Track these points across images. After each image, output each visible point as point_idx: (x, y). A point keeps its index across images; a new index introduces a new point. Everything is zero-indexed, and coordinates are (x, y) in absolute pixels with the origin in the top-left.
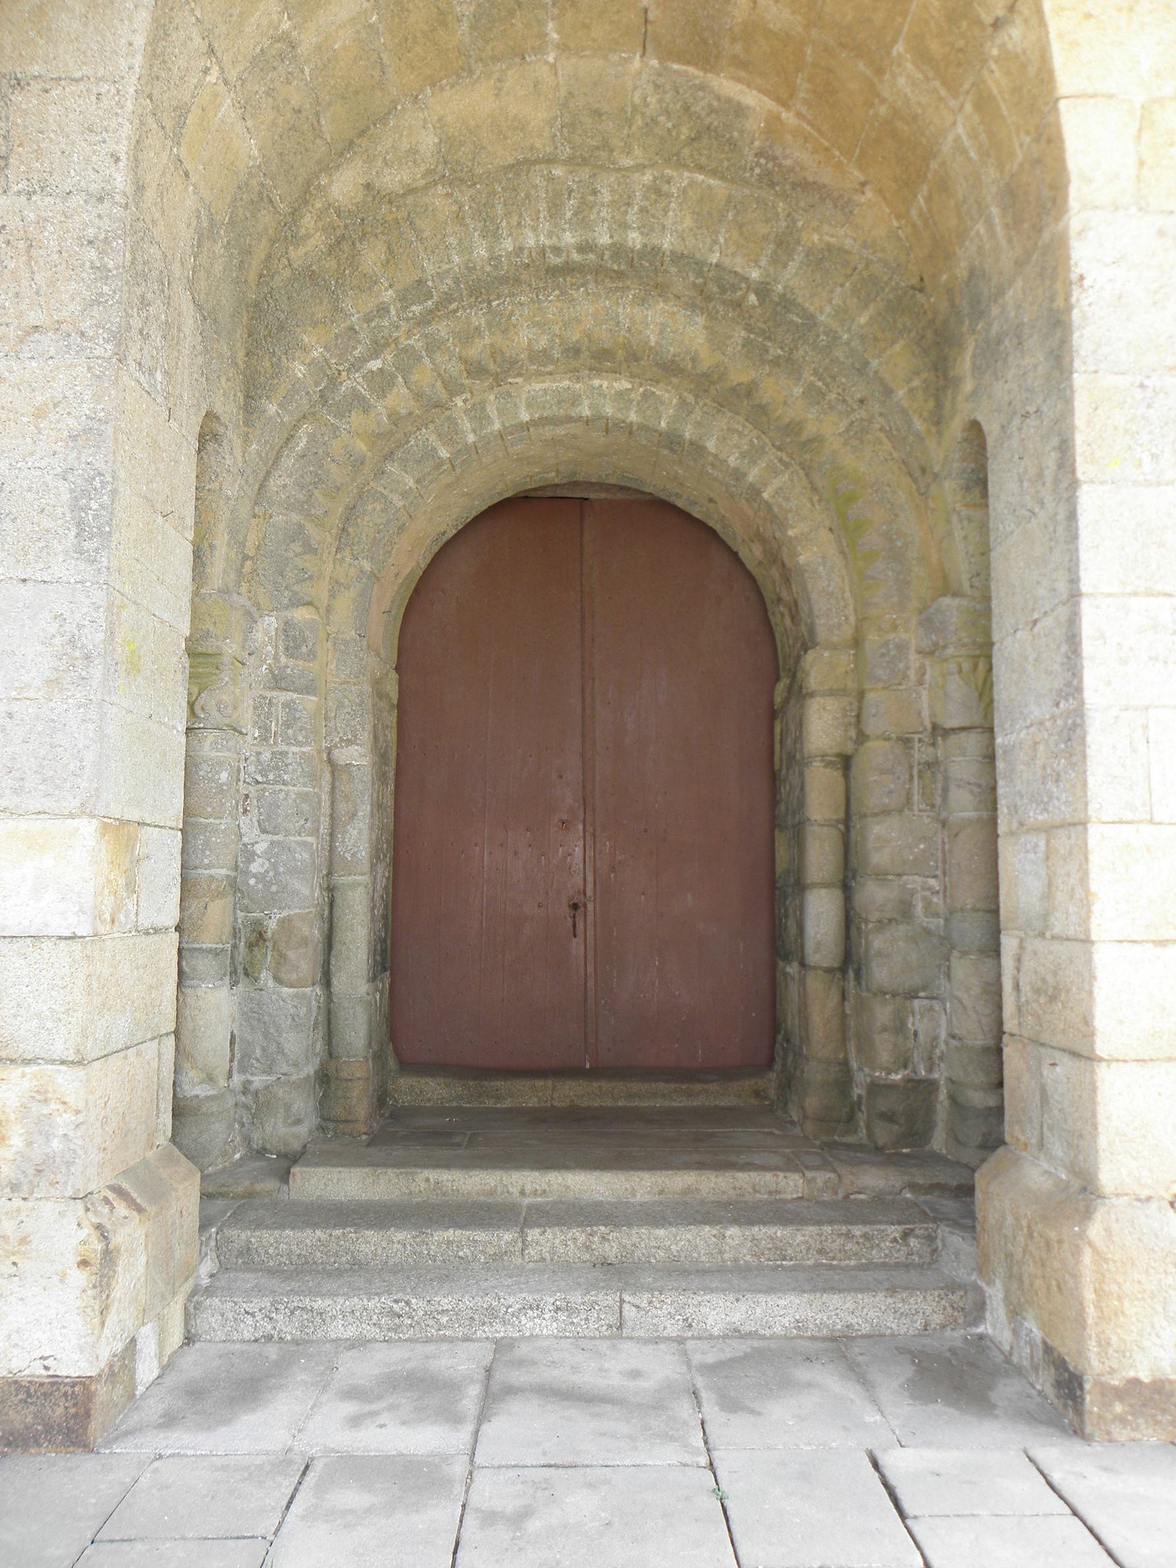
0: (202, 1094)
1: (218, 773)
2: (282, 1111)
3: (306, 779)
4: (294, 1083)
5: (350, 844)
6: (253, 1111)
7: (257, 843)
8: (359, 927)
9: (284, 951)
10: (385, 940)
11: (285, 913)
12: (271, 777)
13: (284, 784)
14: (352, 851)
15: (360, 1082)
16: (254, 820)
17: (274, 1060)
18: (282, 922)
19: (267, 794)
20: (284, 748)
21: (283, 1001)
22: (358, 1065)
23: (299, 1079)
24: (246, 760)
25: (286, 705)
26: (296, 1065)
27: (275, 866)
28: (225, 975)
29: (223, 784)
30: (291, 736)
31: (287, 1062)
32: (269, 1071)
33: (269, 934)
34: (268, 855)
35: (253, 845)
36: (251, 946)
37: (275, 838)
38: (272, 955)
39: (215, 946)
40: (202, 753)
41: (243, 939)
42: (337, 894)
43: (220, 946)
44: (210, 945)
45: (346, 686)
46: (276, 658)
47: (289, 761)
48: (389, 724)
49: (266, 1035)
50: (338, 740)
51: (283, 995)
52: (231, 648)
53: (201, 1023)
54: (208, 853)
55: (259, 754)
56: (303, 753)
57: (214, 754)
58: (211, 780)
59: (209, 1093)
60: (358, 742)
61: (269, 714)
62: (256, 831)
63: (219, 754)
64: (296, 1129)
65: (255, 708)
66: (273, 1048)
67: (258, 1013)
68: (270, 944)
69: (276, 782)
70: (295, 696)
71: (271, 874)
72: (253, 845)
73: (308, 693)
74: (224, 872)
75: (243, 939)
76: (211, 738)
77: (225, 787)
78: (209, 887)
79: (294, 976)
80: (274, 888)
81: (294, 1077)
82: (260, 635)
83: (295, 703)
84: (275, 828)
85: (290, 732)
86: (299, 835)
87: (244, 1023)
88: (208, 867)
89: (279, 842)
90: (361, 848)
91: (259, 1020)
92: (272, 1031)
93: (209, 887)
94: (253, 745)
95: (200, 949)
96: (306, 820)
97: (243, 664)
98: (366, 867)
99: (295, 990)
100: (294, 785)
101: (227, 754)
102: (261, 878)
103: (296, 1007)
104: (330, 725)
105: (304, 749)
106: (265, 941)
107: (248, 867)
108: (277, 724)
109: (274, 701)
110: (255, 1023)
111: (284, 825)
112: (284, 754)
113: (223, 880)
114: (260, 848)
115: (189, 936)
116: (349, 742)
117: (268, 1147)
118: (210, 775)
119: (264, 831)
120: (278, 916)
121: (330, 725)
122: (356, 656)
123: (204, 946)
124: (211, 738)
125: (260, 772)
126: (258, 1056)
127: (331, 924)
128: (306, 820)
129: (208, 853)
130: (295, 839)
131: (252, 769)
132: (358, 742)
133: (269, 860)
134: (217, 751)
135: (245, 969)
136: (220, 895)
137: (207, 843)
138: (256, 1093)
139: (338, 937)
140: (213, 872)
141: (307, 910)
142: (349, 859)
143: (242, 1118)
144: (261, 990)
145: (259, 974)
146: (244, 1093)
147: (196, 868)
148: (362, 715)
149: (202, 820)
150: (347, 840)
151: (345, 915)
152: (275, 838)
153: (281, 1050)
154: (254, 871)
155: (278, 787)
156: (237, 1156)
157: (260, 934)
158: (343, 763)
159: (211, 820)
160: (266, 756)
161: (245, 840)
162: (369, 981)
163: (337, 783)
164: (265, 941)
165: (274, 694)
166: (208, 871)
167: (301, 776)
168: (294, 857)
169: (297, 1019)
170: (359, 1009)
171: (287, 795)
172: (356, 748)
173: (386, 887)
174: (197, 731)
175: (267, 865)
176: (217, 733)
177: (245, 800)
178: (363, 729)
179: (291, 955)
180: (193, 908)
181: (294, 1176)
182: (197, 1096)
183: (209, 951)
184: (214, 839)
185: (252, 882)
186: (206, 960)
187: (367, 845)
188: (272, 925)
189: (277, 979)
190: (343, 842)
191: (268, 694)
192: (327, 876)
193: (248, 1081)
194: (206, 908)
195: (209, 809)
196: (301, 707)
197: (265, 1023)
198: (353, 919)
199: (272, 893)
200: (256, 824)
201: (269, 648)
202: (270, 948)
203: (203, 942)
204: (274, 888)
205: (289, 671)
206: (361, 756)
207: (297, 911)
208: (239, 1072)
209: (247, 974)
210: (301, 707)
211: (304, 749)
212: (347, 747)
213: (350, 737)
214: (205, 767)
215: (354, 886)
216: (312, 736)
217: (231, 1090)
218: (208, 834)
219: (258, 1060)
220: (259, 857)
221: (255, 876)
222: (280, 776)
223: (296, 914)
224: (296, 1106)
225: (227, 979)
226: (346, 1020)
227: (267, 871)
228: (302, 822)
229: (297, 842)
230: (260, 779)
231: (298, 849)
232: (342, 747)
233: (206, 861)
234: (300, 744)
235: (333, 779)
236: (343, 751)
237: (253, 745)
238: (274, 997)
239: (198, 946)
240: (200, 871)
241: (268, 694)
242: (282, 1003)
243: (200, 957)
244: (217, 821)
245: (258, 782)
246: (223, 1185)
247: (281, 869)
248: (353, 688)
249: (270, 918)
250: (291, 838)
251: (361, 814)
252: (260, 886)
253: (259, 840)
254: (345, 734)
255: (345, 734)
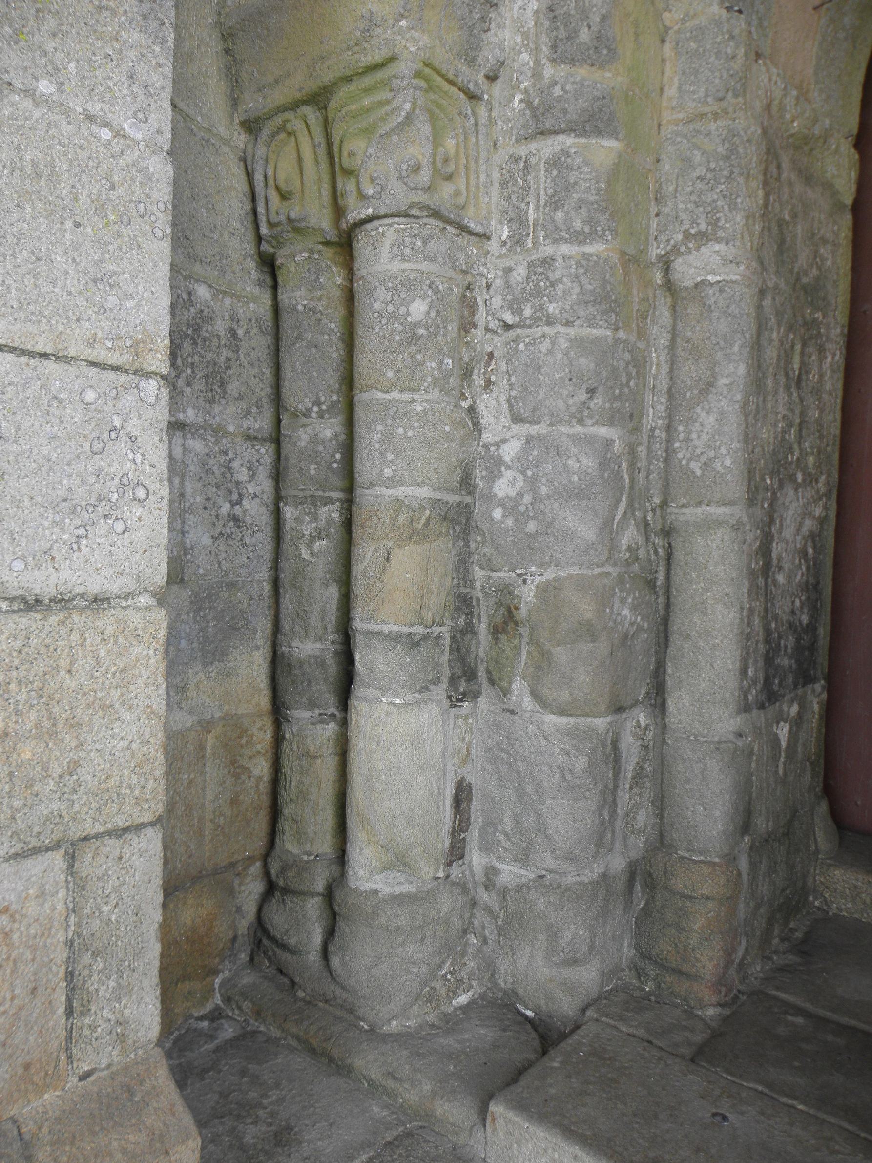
0: (386, 890)
1: (406, 303)
2: (542, 937)
3: (591, 309)
4: (568, 889)
5: (699, 443)
6: (500, 922)
7: (504, 441)
8: (720, 607)
9: (548, 646)
10: (812, 628)
11: (550, 574)
12: (528, 312)
13: (549, 323)
14: (704, 458)
15: (711, 904)
16: (503, 398)
17: (530, 843)
18: (545, 590)
19: (522, 346)
20: (549, 250)
21: (546, 738)
22: (706, 870)
23: (580, 883)
24: (488, 287)
25: (554, 163)
26: (570, 858)
27: (532, 484)
28: (436, 682)
29: (416, 325)
30: (560, 224)
31: (553, 851)
32: (524, 858)
33: (523, 612)
34: (522, 463)
35: (498, 445)
36: (496, 631)
37: (534, 430)
38: (529, 652)
39: (406, 630)
40: (378, 268)
41: (484, 619)
42: (677, 543)
43: (420, 630)
44: (396, 628)
45: (697, 125)
46: (537, 75)
47: (558, 274)
48: (829, 236)
49: (521, 794)
50: (680, 237)
51: (545, 727)
52: (415, 41)
53: (381, 766)
54: (390, 456)
55: (508, 270)
56: (586, 256)
57: (397, 266)
58: (394, 317)
59: (398, 890)
60: (721, 234)
61: (526, 189)
62: (505, 420)
63: (407, 266)
64: (568, 973)
65: (504, 184)
66: (530, 821)
67: (508, 753)
68: (524, 631)
69: (535, 321)
70: (569, 141)
71: (527, 499)
72: (498, 445)
73: (598, 132)
74: (424, 492)
75: (484, 619)
76: (391, 235)
77: (421, 331)
78: (394, 520)
79: (564, 696)
80: (532, 527)
81: (571, 879)
82: (507, 34)
83: (568, 155)
84: (534, 410)
85: (559, 215)
86: (581, 422)
87: (489, 767)
88: (392, 483)
89: (540, 437)
90: (723, 451)
91: (510, 765)
92: (529, 789)
93: (394, 520)
94: (500, 257)
95: (378, 633)
96: (592, 391)
97: (472, 97)
98: (736, 488)
99: (572, 720)
100: (568, 324)
101: (424, 266)
102: (511, 506)
103: (568, 754)
104: (666, 210)
105: (588, 249)
106: (517, 624)
107: (491, 488)
108: (537, 207)
109: (533, 160)
110: (504, 769)
111: (548, 403)
112: (548, 262)
113: (422, 508)
114: (510, 451)
115: (363, 608)
116: (703, 238)
117: (521, 992)
118: (390, 308)
119: (517, 419)
120: (537, 579)
121: (666, 210)
122: (718, 54)
123: (386, 629)
124: (391, 235)
125: (510, 307)
126: (508, 829)
127: (668, 598)
128: (592, 391)
129: (390, 456)
130: (571, 431)
131: (497, 302)
132: (721, 234)
133: (523, 473)
134: (404, 260)
135: (488, 672)
136: (415, 535)
137: (388, 438)
138: (504, 893)
139: (678, 623)
140: (401, 492)
141: (597, 571)
142: (698, 473)
143: (484, 928)
144: (512, 712)
145: (510, 683)
146: (486, 888)
147: (372, 485)
148: (729, 178)
149: (380, 395)
150: (694, 436)
151: (691, 582)
152: (534, 430)
153: (542, 829)
154: (501, 494)
155: (538, 331)
156: (463, 999)
157: (510, 611)
158: (689, 283)
159: (395, 394)
160: (520, 272)
161: (487, 437)
162: (739, 712)
163: (680, 326)
164: (517, 624)
165: (533, 146)
166: (390, 492)
167: (579, 303)
168: (565, 466)
169: (569, 777)
170: (714, 765)
171: (553, 343)
172: (717, 247)
173: (814, 537)
174: (369, 226)
175: (520, 483)
176: (401, 223)
177: (488, 363)
178: (733, 206)
179: (561, 654)
180: (368, 557)
181: (494, 1120)
182: (376, 892)
183: (396, 638)
184: (401, 431)
185: (497, 514)
186: (390, 655)
187: (736, 445)
188: (528, 594)
189: (536, 696)
190: (688, 440)
191: (522, 151)
192: (661, 507)
193: (493, 868)
194: (388, 559)
195: (390, 374)
196: (579, 160)
197: (518, 773)
198: (707, 590)
199: (529, 536)
200: (506, 406)
201: (525, 57)
202: (526, 640)
203: (383, 622)
204: (532, 527)
205: (557, 91)
206: (726, 262)
207: (574, 571)
208: (480, 849)
209: (492, 682)
210: (579, 160)
211: (588, 249)
212: (698, 249)
213: (703, 227)
214: (382, 294)
215: (709, 525)
216: (603, 219)
217: (453, 884)
218: (389, 422)
219: (506, 834)
220: (508, 468)
221: (502, 504)
222: (541, 307)
223: (570, 577)
224: (568, 935)
225: (440, 691)
226: (688, 781)
227: (520, 495)
228: (583, 396)
229: (576, 439)
230: (509, 318)
231: (574, 450)
232: (689, 251)
233: (388, 472)
234: (579, 238)
235: (675, 320)
236: (691, 258)
237: (500, 257)
238: (531, 728)
239: (375, 628)
240: (378, 490)
241: (522, 151)
242: (544, 743)
243: (380, 646)
244: (406, 396)
245: (507, 327)
246: (392, 1075)
247: (544, 490)
248: (713, 126)
249: (525, 581)
250: (564, 429)
251: (723, 381)
252: (510, 522)
253: (508, 435)
254: (694, 222)
255: (694, 222)
